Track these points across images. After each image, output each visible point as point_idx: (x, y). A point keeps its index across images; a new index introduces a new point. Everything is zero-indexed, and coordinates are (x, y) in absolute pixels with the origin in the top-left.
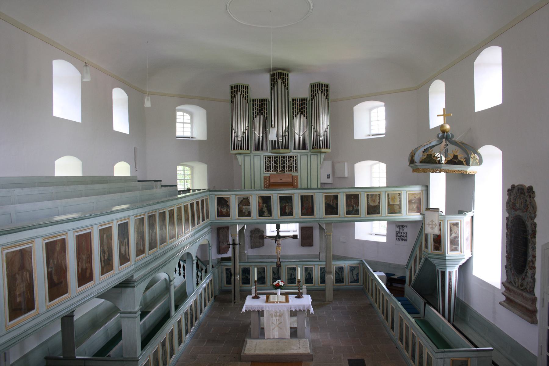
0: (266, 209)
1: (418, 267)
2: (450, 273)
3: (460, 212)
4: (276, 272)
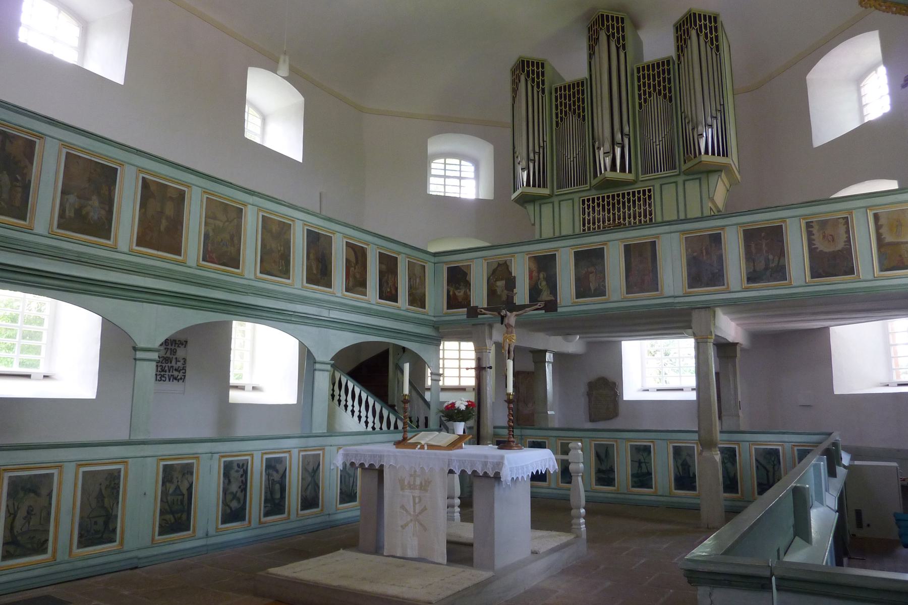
0: (544, 283)
4: (603, 456)
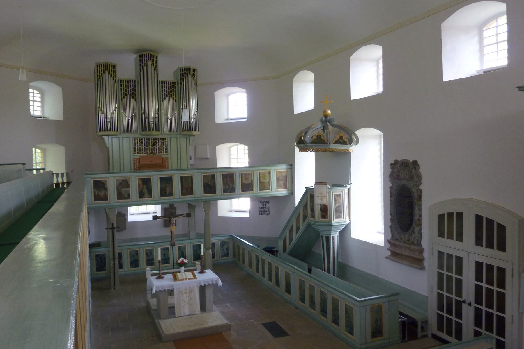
0: (146, 190)
1: (295, 237)
2: (333, 237)
3: (342, 186)
